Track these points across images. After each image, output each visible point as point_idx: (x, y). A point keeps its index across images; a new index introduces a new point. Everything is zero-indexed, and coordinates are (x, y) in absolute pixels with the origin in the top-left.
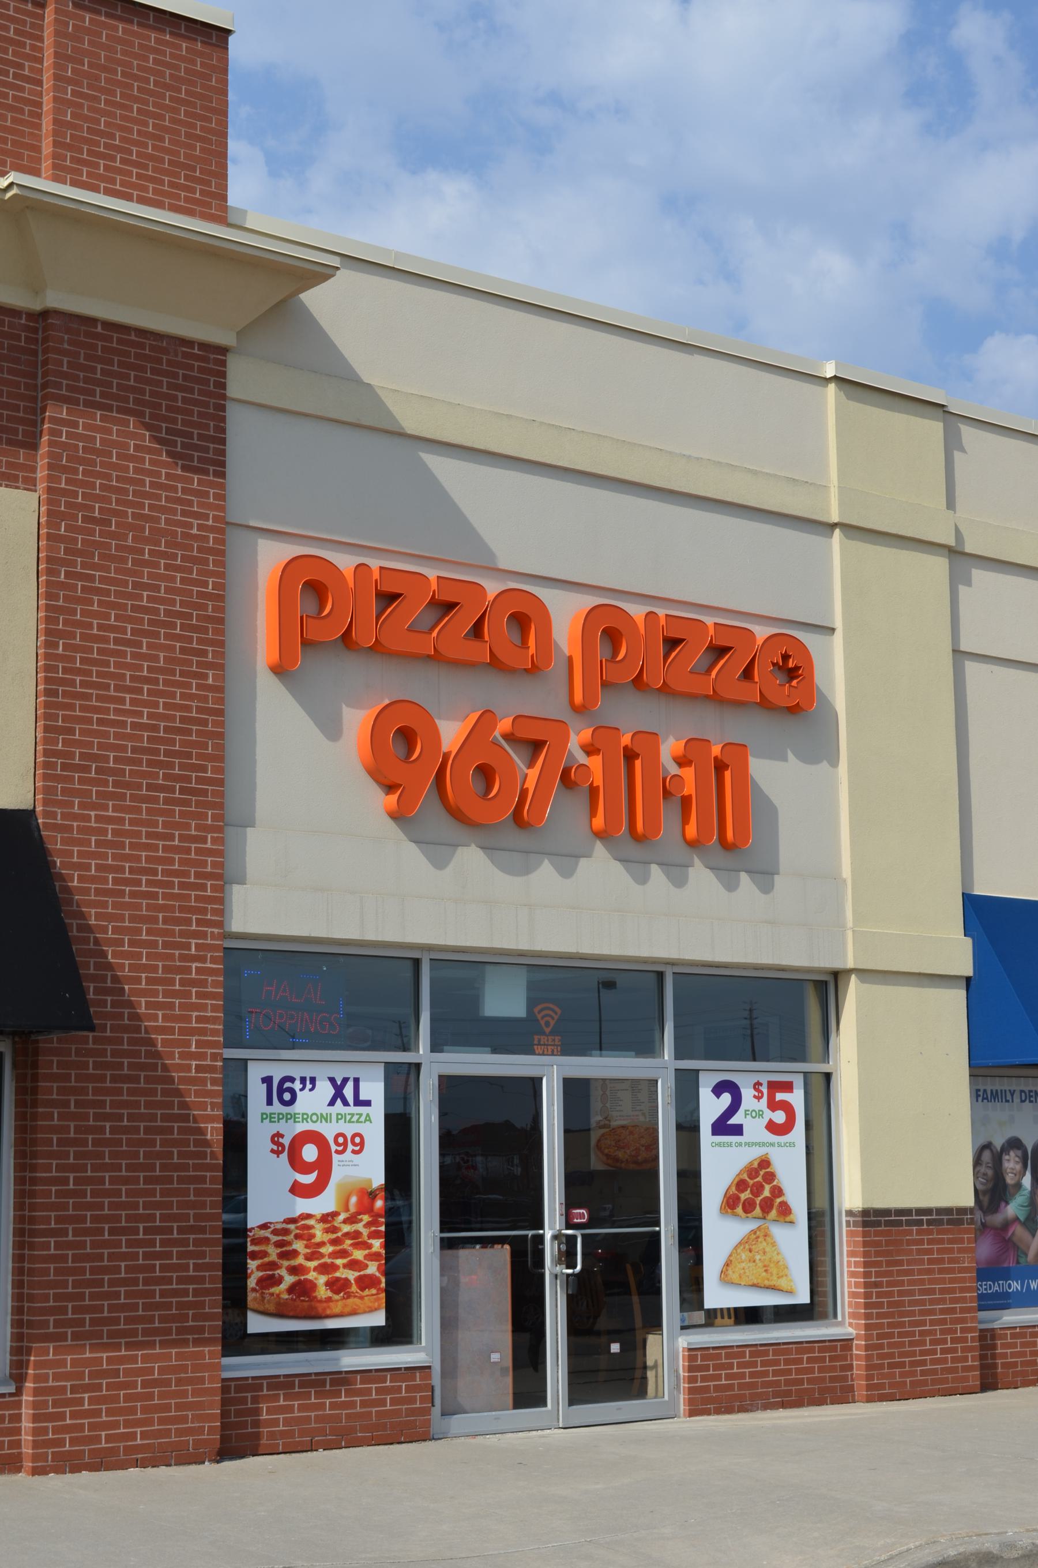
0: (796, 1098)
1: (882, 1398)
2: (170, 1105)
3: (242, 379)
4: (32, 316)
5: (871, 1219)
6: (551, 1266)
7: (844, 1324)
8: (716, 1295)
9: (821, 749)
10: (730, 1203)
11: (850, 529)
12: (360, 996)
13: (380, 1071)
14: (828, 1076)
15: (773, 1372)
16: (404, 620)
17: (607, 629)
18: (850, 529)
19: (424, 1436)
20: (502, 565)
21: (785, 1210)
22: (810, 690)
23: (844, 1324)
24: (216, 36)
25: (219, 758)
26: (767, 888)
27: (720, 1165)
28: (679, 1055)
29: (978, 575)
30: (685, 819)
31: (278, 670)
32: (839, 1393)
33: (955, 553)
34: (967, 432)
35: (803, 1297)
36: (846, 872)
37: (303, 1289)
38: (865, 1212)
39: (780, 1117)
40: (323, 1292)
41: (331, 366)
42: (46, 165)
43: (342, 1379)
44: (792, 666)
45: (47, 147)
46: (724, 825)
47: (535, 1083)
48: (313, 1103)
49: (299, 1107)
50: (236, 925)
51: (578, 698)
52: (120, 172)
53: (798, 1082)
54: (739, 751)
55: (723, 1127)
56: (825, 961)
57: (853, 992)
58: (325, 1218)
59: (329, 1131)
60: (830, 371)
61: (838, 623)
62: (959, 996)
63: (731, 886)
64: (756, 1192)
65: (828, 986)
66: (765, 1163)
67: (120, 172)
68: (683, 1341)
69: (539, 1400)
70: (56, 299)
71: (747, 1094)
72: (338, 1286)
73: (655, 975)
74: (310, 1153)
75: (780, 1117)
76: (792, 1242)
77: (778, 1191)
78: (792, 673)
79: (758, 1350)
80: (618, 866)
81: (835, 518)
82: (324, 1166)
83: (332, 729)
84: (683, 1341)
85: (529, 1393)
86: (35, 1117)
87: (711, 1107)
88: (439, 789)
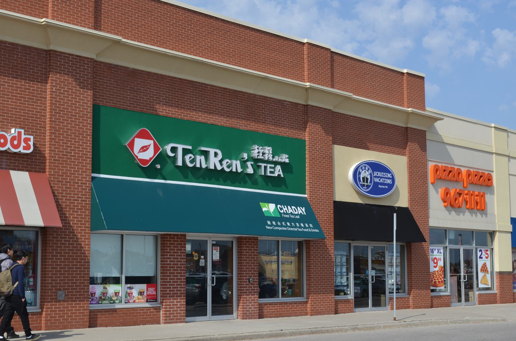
0: (489, 252)
1: (502, 303)
2: (85, 259)
3: (428, 136)
4: (46, 51)
5: (501, 273)
6: (462, 280)
7: (495, 291)
8: (481, 286)
9: (492, 193)
10: (481, 270)
11: (497, 154)
12: (441, 235)
13: (442, 248)
14: (492, 249)
15: (487, 299)
16: (448, 174)
17: (469, 174)
18: (497, 154)
19: (450, 306)
20: (455, 163)
21: (488, 271)
22: (492, 183)
23: (495, 291)
24: (422, 78)
25: (427, 198)
26: (486, 217)
27: (480, 263)
28: (476, 245)
29: (511, 160)
30: (467, 204)
31: (432, 183)
32: (495, 302)
33: (509, 156)
34: (510, 134)
35: (490, 286)
36: (496, 214)
37: (435, 282)
38: (499, 272)
39: (487, 256)
40: (437, 283)
41: (437, 133)
42: (405, 103)
43: (441, 296)
44: (490, 179)
45: (406, 100)
46: (479, 206)
47: (459, 250)
48: (436, 252)
49: (434, 254)
50: (430, 225)
51: (465, 185)
52: (76, 13)
53: (489, 250)
54: (484, 193)
55: (481, 258)
56: (491, 228)
57: (497, 235)
58: (438, 271)
59: (437, 257)
60: (493, 125)
61: (494, 170)
62: (510, 235)
63: (472, 216)
64: (484, 269)
65: (492, 234)
66: (485, 263)
67: (76, 13)
68: (477, 293)
69: (393, 309)
70: (52, 47)
71: (483, 252)
72: (439, 282)
73: (472, 232)
74: (435, 261)
75: (487, 256)
76: (488, 276)
77: (487, 268)
78: (489, 180)
79: (486, 294)
80: (447, 212)
81: (494, 152)
82: (437, 263)
83: (437, 193)
84: (477, 293)
85: (460, 301)
86: (45, 262)
87: (479, 254)
88: (451, 203)
